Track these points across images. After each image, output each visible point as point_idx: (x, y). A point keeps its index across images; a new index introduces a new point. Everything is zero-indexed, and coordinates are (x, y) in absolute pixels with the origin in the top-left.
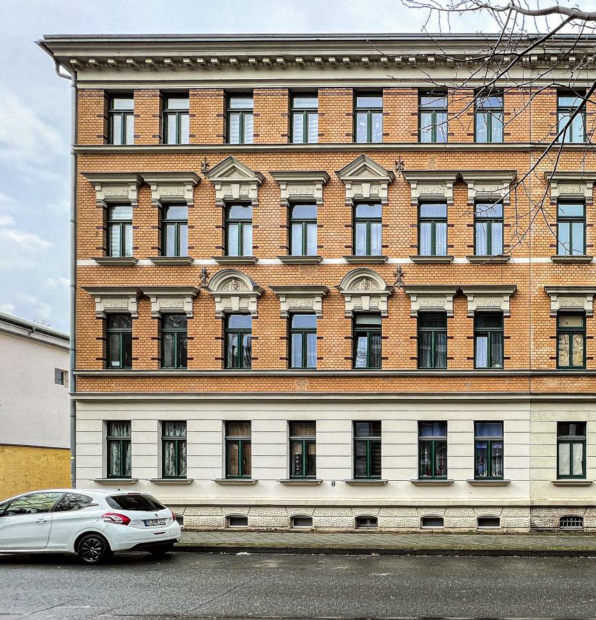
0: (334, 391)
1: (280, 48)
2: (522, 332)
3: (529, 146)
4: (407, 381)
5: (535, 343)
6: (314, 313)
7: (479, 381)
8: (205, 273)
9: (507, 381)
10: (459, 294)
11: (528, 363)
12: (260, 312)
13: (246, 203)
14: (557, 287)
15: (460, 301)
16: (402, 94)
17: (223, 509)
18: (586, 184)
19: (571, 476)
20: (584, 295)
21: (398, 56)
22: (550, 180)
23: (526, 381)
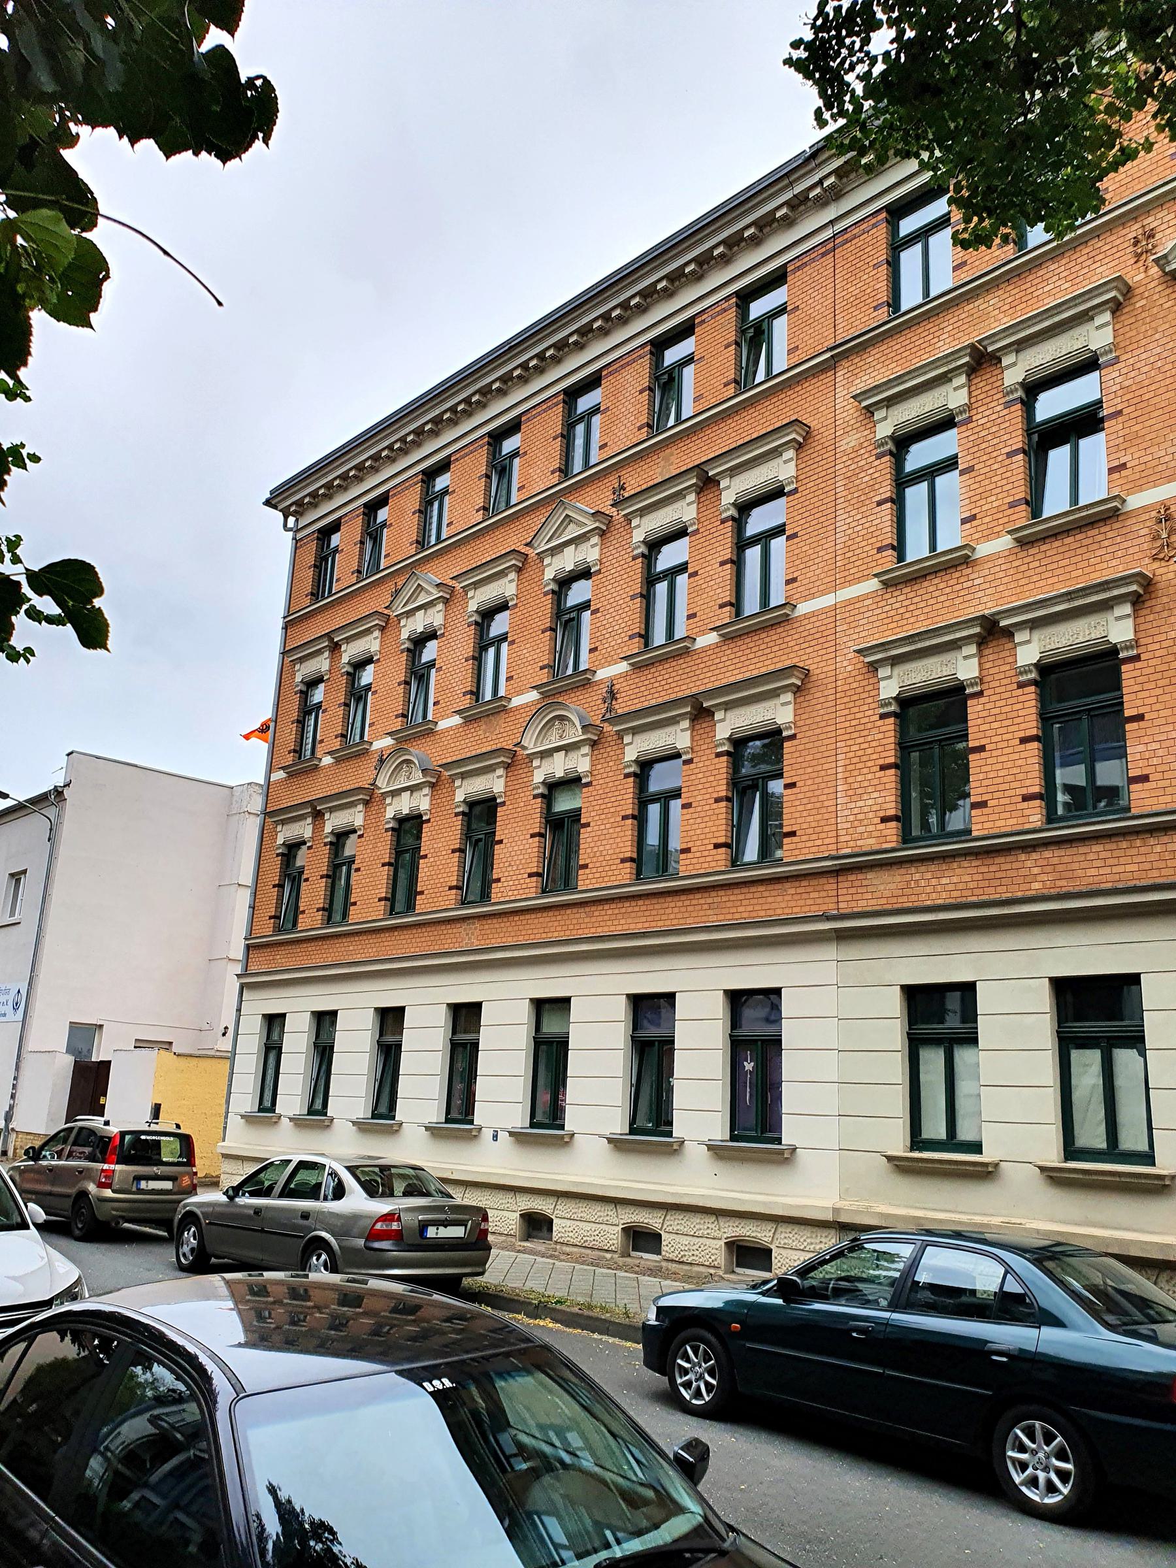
0: (510, 941)
1: (441, 401)
2: (819, 768)
3: (828, 355)
4: (610, 910)
5: (846, 787)
6: (677, 755)
7: (736, 895)
8: (612, 692)
9: (790, 888)
10: (992, 632)
11: (834, 840)
12: (697, 749)
13: (585, 573)
14: (1069, 593)
15: (704, 725)
16: (628, 364)
17: (722, 1220)
18: (950, 380)
19: (1113, 1152)
20: (955, 645)
21: (633, 296)
22: (871, 405)
23: (830, 885)
